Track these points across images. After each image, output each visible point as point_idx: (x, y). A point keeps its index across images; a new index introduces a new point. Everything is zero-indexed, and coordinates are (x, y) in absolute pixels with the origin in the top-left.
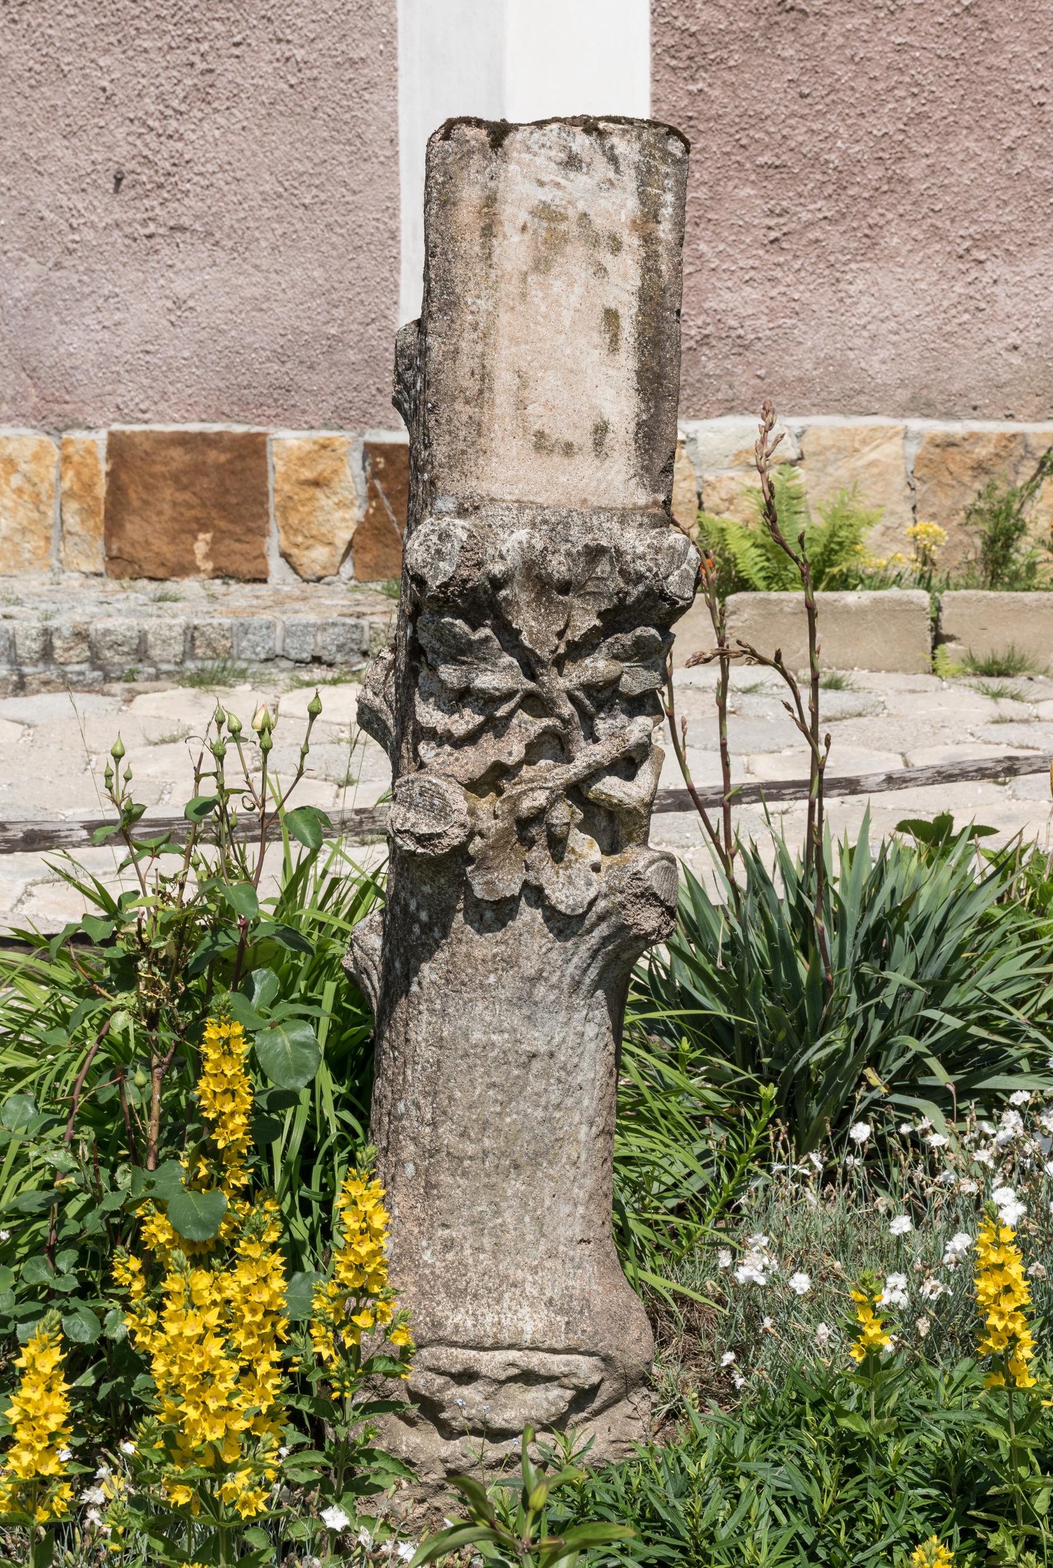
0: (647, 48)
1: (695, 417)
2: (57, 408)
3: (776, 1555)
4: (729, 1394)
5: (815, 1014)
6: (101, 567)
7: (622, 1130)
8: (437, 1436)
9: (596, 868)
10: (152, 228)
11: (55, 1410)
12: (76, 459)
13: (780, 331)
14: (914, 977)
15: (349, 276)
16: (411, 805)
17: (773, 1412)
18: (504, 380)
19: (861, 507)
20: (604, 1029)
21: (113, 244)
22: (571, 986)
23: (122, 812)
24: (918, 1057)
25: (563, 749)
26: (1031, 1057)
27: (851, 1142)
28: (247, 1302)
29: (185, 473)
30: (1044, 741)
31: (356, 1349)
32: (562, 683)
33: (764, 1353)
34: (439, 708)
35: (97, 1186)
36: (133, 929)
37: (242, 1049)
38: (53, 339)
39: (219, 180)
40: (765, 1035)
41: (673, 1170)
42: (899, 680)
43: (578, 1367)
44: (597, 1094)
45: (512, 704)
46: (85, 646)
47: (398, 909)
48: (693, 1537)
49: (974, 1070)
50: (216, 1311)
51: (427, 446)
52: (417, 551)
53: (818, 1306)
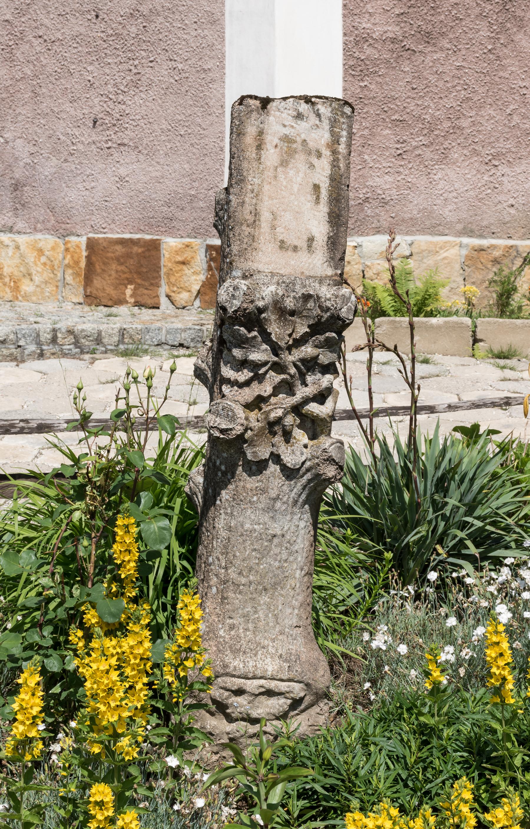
0: (341, 66)
1: (361, 235)
2: (63, 226)
3: (388, 784)
4: (367, 704)
5: (413, 518)
6: (82, 301)
7: (318, 573)
8: (225, 721)
9: (306, 446)
10: (110, 144)
11: (36, 705)
12: (72, 249)
13: (402, 196)
14: (460, 501)
15: (201, 167)
16: (218, 415)
17: (388, 713)
18: (265, 216)
19: (439, 278)
20: (308, 524)
21: (92, 151)
22: (293, 502)
23: (81, 415)
24: (461, 540)
25: (290, 390)
26: (516, 541)
27: (428, 581)
28: (132, 653)
29: (123, 257)
30: (525, 389)
31: (185, 677)
32: (291, 358)
33: (385, 683)
34: (232, 369)
35: (63, 595)
36: (85, 471)
37: (134, 530)
38: (62, 194)
39: (142, 123)
40: (388, 528)
41: (342, 593)
42: (456, 360)
43: (293, 688)
44: (305, 555)
45: (267, 368)
46: (72, 337)
47: (211, 464)
48: (348, 774)
49: (488, 546)
50: (116, 658)
51: (229, 246)
52: (223, 294)
53: (412, 660)
